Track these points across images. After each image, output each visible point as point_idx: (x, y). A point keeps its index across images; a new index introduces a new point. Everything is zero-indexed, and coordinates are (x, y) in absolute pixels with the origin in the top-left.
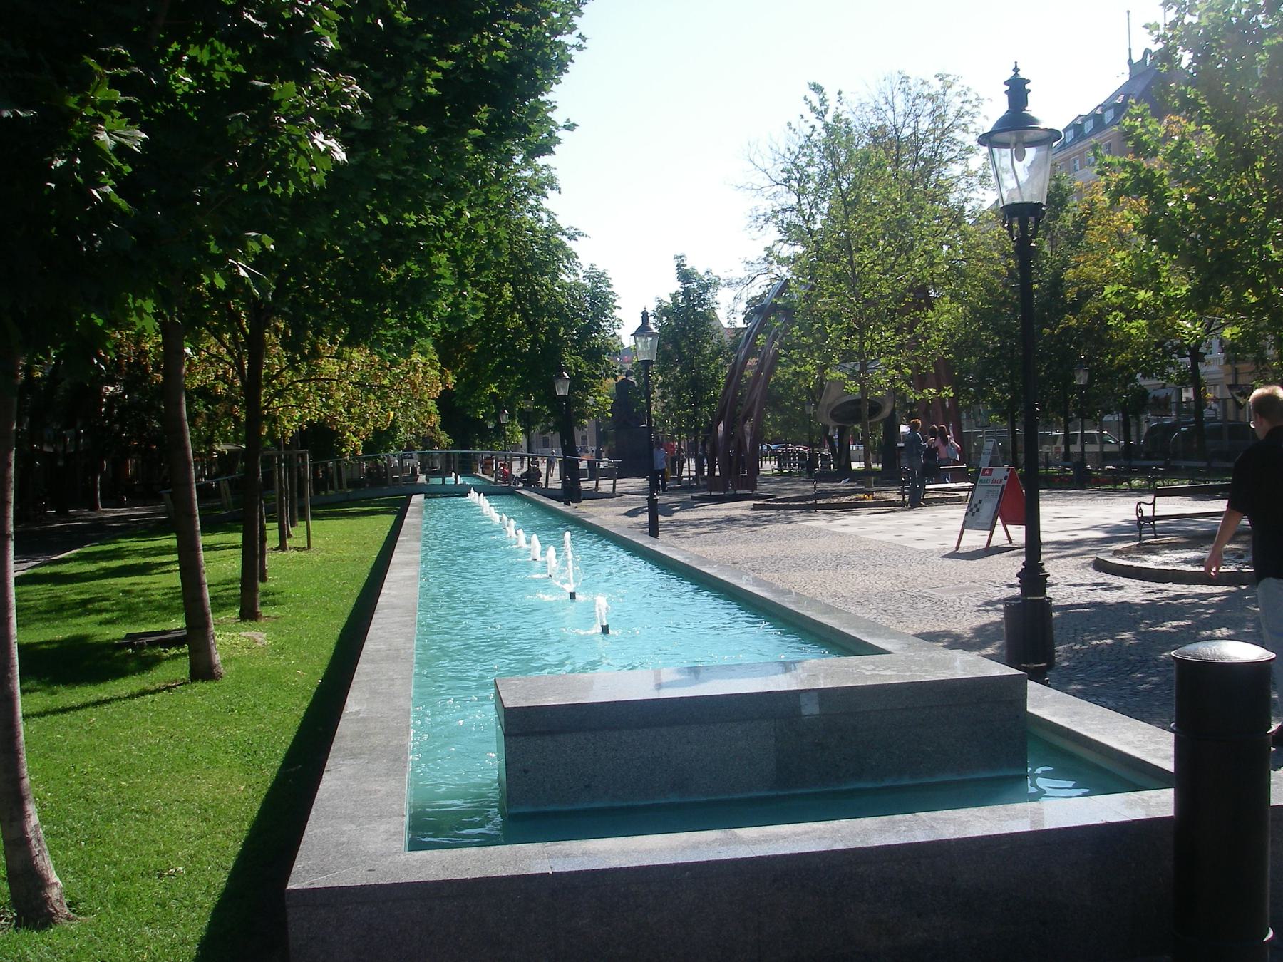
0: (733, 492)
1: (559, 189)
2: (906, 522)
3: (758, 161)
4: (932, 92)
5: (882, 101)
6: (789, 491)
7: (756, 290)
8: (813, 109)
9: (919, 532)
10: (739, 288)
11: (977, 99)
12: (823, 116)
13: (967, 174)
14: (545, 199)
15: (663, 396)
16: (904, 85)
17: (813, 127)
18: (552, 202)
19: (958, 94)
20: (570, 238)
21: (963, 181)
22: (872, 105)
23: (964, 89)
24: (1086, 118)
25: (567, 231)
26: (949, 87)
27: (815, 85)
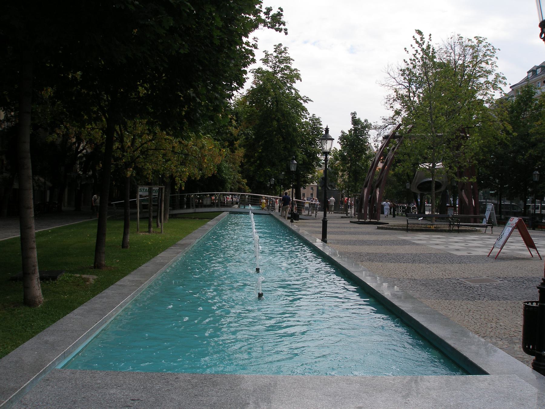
0: (369, 220)
1: (301, 79)
2: (450, 240)
3: (392, 74)
4: (473, 44)
5: (450, 48)
6: (392, 222)
7: (388, 132)
8: (417, 42)
9: (457, 246)
10: (380, 130)
11: (493, 49)
12: (422, 46)
13: (488, 82)
14: (294, 83)
15: (343, 175)
16: (460, 41)
17: (417, 51)
18: (297, 85)
19: (485, 47)
20: (305, 101)
21: (485, 86)
22: (445, 49)
23: (487, 44)
24: (538, 67)
25: (303, 98)
26: (481, 43)
27: (418, 30)
